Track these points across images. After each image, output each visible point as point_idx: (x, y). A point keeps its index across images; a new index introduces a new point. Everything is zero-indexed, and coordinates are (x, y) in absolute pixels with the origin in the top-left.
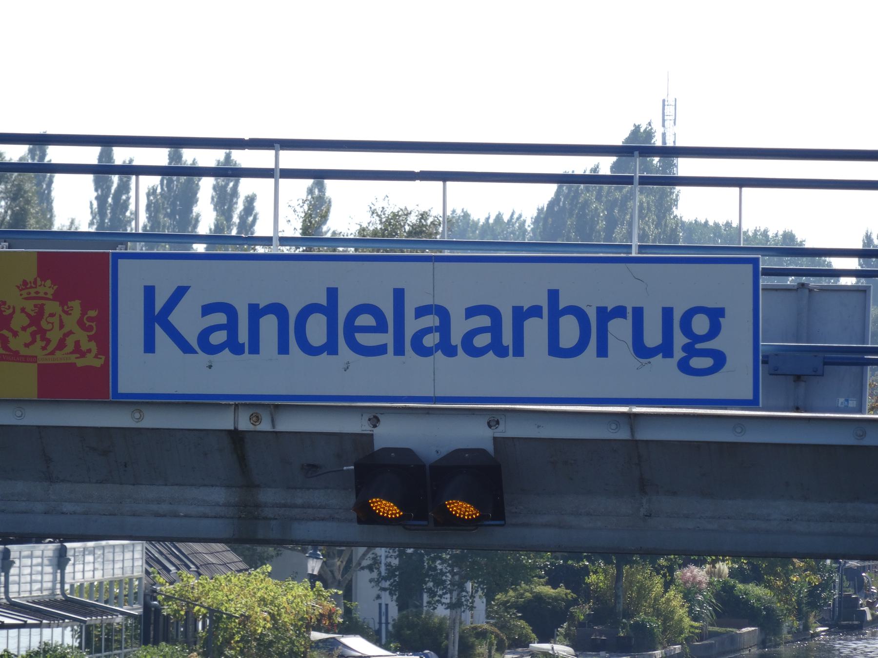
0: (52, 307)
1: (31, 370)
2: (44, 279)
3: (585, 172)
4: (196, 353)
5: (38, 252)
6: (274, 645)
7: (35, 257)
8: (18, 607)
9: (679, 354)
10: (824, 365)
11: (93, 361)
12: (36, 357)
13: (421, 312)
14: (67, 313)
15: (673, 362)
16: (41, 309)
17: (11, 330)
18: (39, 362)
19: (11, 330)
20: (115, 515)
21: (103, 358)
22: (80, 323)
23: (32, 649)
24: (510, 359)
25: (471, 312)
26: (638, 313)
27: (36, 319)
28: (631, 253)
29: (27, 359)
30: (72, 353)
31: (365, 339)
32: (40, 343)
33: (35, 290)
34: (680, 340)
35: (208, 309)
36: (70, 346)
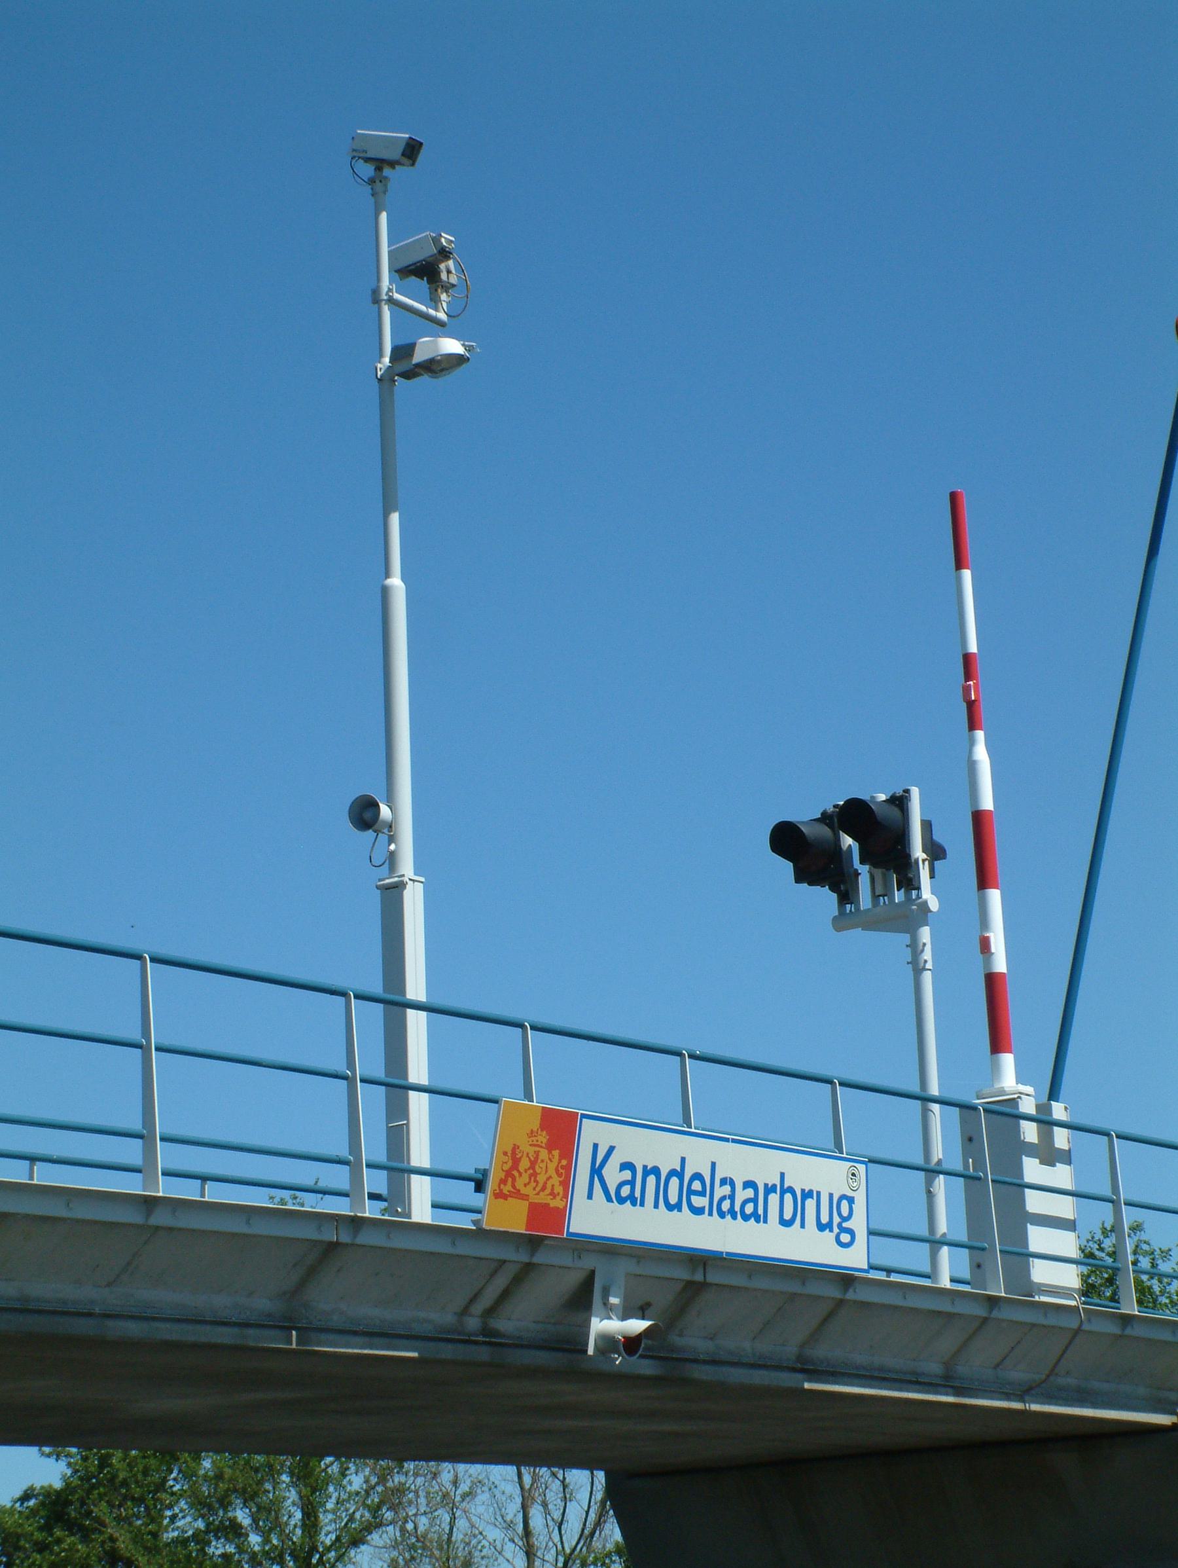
0: (544, 1154)
1: (523, 1207)
2: (542, 1130)
4: (613, 1202)
5: (543, 1107)
6: (50, 1506)
7: (541, 1108)
8: (808, 1369)
9: (836, 1230)
10: (1074, 1222)
11: (557, 1203)
12: (528, 1196)
13: (723, 1182)
14: (551, 1161)
15: (833, 1235)
16: (537, 1154)
17: (518, 1171)
18: (530, 1201)
19: (518, 1171)
21: (565, 1200)
22: (557, 1170)
26: (819, 1193)
27: (533, 1164)
28: (366, 1213)
29: (525, 1197)
30: (548, 1195)
31: (698, 1201)
32: (533, 1184)
33: (536, 1138)
36: (548, 1191)
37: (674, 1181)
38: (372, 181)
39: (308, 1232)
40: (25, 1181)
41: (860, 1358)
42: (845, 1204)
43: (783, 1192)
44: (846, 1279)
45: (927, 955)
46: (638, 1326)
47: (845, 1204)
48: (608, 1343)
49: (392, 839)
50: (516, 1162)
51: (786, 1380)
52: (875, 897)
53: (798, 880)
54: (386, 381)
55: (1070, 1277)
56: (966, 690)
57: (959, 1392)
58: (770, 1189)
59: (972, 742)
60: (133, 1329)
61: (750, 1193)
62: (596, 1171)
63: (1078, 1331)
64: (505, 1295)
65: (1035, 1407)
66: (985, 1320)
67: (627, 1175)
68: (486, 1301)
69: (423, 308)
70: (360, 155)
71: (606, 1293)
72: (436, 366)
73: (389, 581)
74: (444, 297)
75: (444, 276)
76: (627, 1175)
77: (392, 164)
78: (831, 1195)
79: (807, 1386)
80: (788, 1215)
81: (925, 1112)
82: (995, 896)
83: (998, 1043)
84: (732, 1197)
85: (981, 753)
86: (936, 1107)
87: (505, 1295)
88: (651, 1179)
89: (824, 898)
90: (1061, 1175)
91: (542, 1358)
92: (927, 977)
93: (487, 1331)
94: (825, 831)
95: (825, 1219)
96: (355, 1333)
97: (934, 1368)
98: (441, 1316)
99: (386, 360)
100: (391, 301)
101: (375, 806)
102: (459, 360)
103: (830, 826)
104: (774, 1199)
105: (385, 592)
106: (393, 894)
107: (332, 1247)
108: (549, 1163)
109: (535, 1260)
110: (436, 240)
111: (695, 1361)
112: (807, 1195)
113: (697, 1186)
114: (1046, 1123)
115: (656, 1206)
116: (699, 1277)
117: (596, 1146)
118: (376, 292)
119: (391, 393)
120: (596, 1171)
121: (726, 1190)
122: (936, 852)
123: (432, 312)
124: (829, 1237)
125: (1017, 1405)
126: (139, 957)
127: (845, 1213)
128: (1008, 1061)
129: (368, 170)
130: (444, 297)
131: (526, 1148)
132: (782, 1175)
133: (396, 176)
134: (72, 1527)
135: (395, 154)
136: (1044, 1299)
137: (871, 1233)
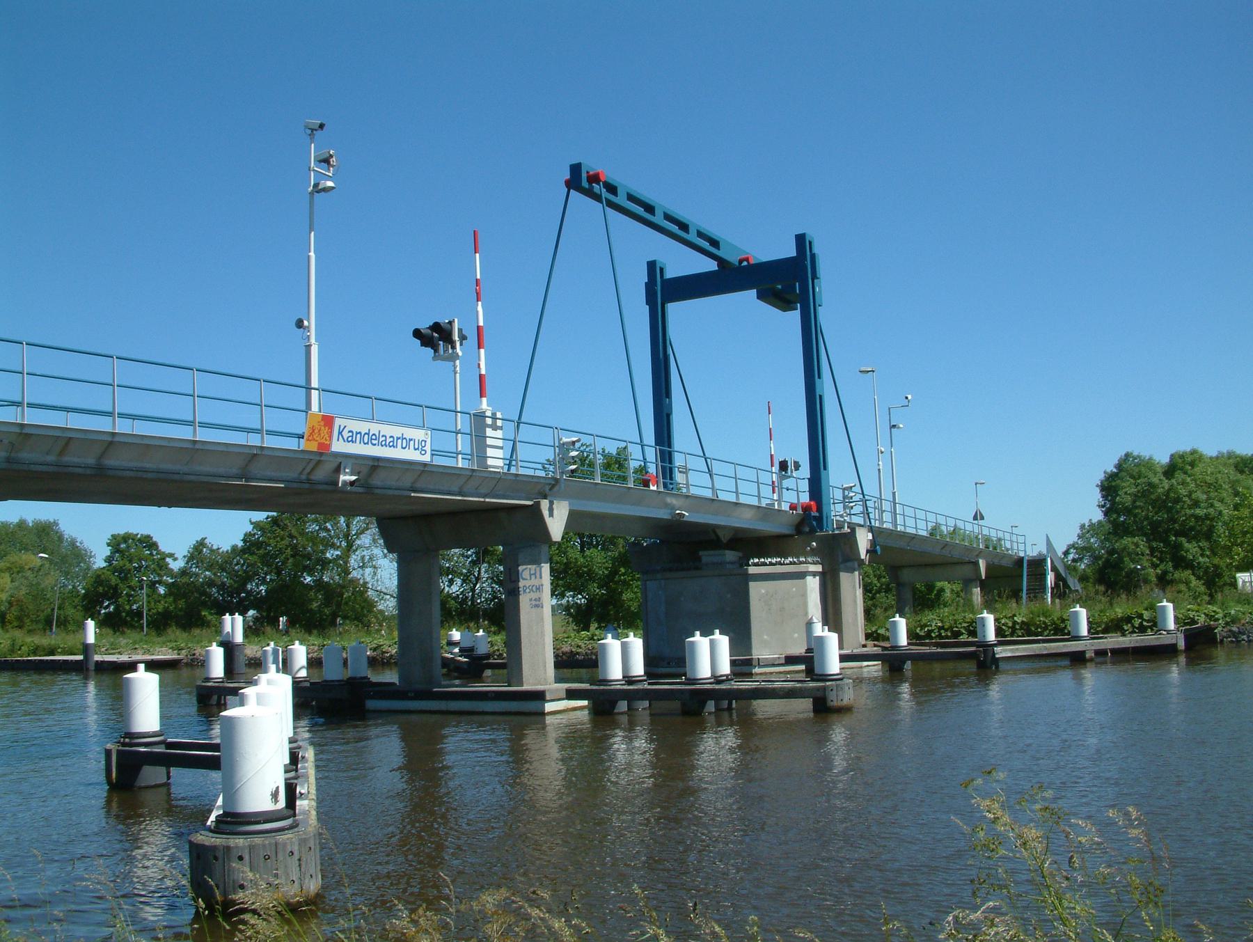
0: (323, 428)
3: (997, 653)
11: (328, 442)
13: (383, 436)
20: (942, 549)
23: (521, 580)
24: (395, 449)
25: (391, 437)
29: (317, 441)
31: (374, 442)
34: (420, 447)
35: (349, 432)
37: (366, 436)
38: (310, 135)
39: (247, 451)
40: (131, 433)
41: (432, 487)
42: (423, 443)
43: (403, 439)
44: (425, 465)
45: (458, 369)
46: (354, 478)
47: (423, 443)
48: (345, 483)
49: (309, 331)
50: (313, 431)
51: (406, 493)
52: (444, 351)
53: (421, 346)
54: (312, 193)
55: (500, 463)
56: (476, 289)
57: (462, 496)
58: (398, 438)
59: (477, 305)
60: (192, 478)
61: (392, 439)
62: (340, 433)
63: (499, 479)
64: (313, 469)
65: (487, 500)
66: (471, 476)
67: (350, 434)
68: (308, 470)
69: (324, 172)
70: (306, 127)
71: (345, 469)
72: (326, 190)
73: (310, 254)
74: (331, 169)
75: (332, 163)
76: (350, 434)
77: (316, 130)
78: (419, 440)
79: (412, 495)
80: (404, 446)
81: (456, 415)
82: (482, 351)
83: (482, 395)
84: (386, 440)
85: (480, 308)
86: (459, 414)
87: (313, 469)
88: (359, 435)
89: (429, 351)
90: (499, 434)
91: (325, 487)
92: (458, 375)
93: (308, 479)
94: (429, 331)
95: (416, 447)
96: (264, 480)
97: (456, 489)
98: (292, 475)
99: (311, 188)
100: (314, 170)
101: (303, 322)
102: (333, 188)
103: (431, 330)
104: (400, 441)
105: (309, 256)
106: (308, 347)
107: (255, 455)
108: (325, 431)
109: (322, 459)
110: (329, 152)
111: (377, 488)
112: (411, 440)
113: (374, 437)
114: (494, 418)
115: (360, 443)
116: (376, 464)
117: (340, 426)
118: (310, 167)
119: (313, 197)
120: (340, 433)
121: (384, 438)
122: (463, 338)
123: (327, 173)
124: (418, 452)
125: (482, 500)
126: (112, 357)
127: (423, 445)
128: (484, 400)
129: (309, 132)
130: (331, 169)
131: (316, 426)
132: (403, 434)
133: (318, 133)
134: (278, 526)
135: (317, 127)
136: (492, 469)
137: (432, 450)
